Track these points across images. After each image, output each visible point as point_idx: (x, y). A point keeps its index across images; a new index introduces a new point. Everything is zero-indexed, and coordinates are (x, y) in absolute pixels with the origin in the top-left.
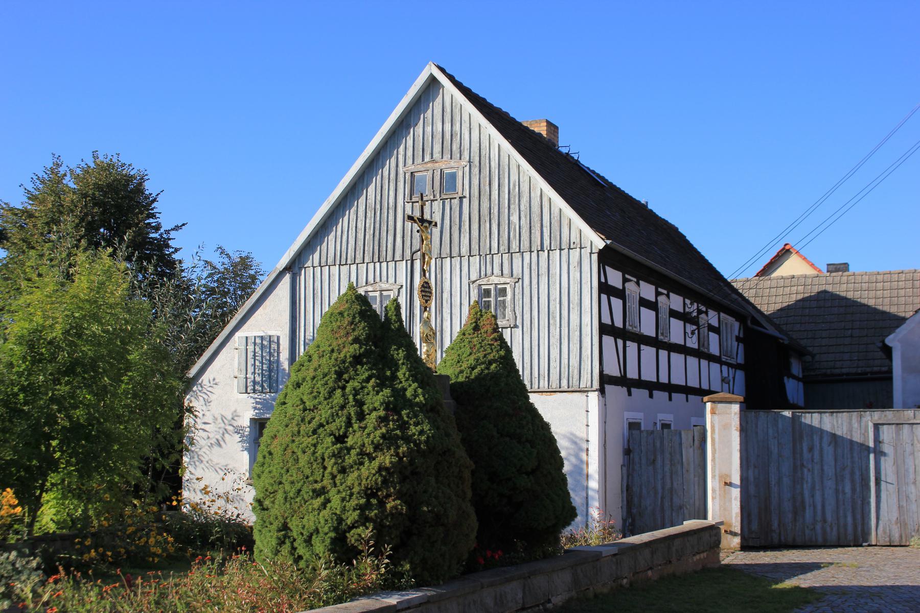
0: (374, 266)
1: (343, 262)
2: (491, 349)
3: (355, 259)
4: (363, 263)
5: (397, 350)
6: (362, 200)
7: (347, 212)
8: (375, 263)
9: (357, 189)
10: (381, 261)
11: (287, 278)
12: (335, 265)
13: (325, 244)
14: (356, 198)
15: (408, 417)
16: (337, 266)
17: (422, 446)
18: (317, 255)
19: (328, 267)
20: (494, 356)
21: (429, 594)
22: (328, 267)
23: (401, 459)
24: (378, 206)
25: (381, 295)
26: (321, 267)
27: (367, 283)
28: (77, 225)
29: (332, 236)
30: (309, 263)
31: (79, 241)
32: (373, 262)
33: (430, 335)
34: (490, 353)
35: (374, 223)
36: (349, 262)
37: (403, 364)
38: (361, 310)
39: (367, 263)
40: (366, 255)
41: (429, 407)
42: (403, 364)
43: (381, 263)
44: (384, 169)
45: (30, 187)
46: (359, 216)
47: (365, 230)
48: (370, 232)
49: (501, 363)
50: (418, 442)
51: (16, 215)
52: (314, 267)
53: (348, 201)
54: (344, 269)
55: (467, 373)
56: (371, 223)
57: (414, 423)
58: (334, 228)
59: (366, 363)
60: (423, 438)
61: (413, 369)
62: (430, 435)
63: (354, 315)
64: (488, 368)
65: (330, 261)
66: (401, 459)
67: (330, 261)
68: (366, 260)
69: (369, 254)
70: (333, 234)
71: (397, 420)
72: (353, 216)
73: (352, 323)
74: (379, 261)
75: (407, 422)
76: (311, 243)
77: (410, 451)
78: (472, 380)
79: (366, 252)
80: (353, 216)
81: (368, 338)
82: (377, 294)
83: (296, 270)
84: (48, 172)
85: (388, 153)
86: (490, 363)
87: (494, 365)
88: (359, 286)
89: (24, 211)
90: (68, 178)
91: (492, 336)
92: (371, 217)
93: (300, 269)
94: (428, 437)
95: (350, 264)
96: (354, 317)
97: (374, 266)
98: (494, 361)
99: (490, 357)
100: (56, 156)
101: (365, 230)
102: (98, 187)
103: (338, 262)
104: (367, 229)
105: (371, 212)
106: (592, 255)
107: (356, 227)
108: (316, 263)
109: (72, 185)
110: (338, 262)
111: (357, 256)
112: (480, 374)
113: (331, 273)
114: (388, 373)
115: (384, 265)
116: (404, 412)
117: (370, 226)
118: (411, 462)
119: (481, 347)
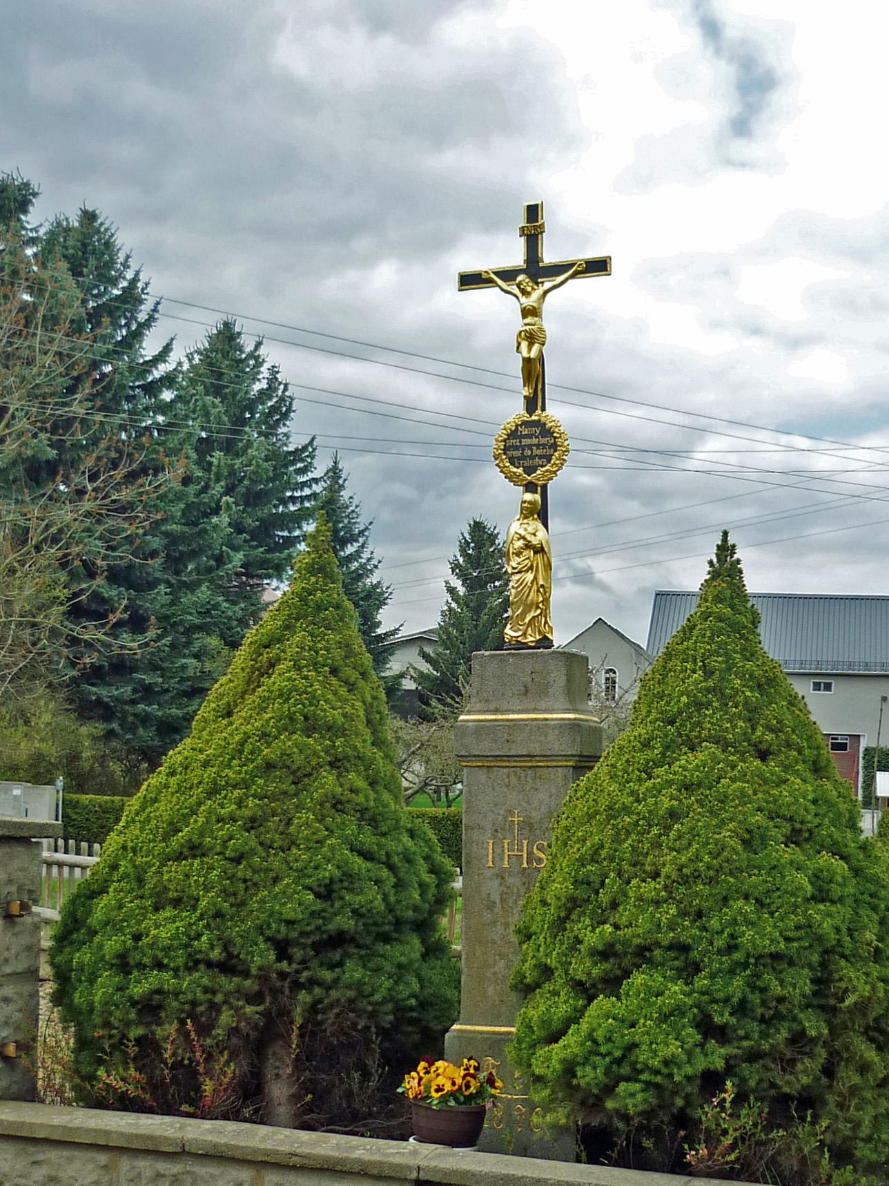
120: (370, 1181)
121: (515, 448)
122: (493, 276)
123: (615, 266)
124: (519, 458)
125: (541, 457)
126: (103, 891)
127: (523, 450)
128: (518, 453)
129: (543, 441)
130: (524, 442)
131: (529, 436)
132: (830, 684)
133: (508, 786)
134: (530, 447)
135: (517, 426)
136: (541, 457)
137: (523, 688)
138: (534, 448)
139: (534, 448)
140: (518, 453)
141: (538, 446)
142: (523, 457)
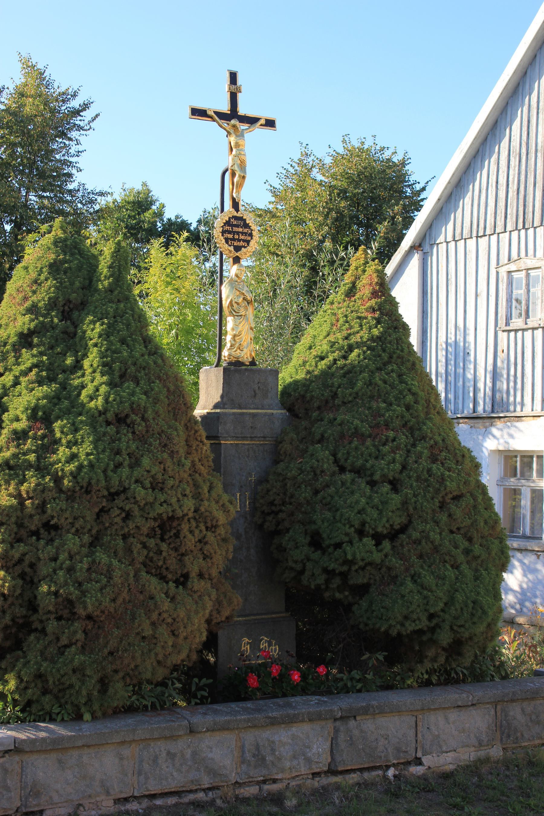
0: (519, 235)
1: (481, 234)
2: (361, 326)
3: (495, 227)
4: (505, 232)
5: (94, 322)
6: (505, 143)
7: (486, 163)
8: (519, 230)
9: (498, 128)
10: (526, 227)
11: (415, 261)
12: (471, 238)
13: (460, 210)
14: (498, 141)
15: (62, 432)
16: (475, 239)
17: (66, 482)
18: (450, 226)
19: (463, 241)
20: (361, 338)
21: (22, 736)
22: (463, 241)
23: (21, 503)
24: (524, 151)
25: (528, 275)
26: (456, 241)
27: (509, 260)
28: (321, 225)
29: (468, 199)
30: (441, 239)
31: (322, 242)
32: (516, 229)
33: (238, 304)
34: (358, 332)
35: (519, 174)
36: (488, 232)
37: (96, 345)
38: (55, 261)
39: (510, 231)
40: (508, 220)
41: (110, 416)
42: (96, 345)
43: (527, 229)
44: (532, 96)
45: (276, 183)
46: (500, 165)
47: (508, 185)
48: (513, 188)
49: (369, 348)
50: (60, 474)
51: (260, 216)
52: (447, 243)
53: (488, 144)
54: (483, 241)
55: (310, 365)
56: (514, 175)
57: (69, 442)
58: (471, 187)
59: (38, 345)
60: (71, 467)
61: (109, 353)
62: (85, 463)
63: (42, 268)
64: (345, 357)
65: (466, 234)
66: (21, 503)
67: (466, 234)
68: (509, 228)
69: (512, 218)
70: (470, 194)
71: (43, 437)
72: (493, 168)
73: (36, 282)
74: (524, 227)
75: (57, 442)
76: (444, 210)
77: (41, 489)
78: (316, 376)
79: (509, 216)
80: (493, 168)
81: (52, 304)
82: (523, 274)
83: (427, 248)
84: (294, 164)
85: (537, 71)
86: (351, 349)
87: (356, 351)
88: (500, 264)
89: (267, 211)
90: (315, 170)
91: (369, 304)
92: (515, 167)
93: (432, 245)
94: (80, 468)
95: (490, 235)
96: (40, 272)
97: (519, 235)
98: (358, 345)
99: (354, 339)
100: (304, 145)
101: (508, 185)
102: (345, 175)
103: (474, 234)
104: (510, 183)
105: (515, 158)
106: (242, 110)
107: (497, 182)
108: (450, 238)
109: (319, 177)
110: (474, 234)
111: (498, 223)
112: (329, 367)
113: (467, 249)
114: (69, 361)
115: (531, 232)
116: (57, 425)
117: (514, 178)
118: (42, 508)
119: (347, 322)
120: (218, 733)
121: (229, 232)
122: (213, 114)
123: (234, 69)
124: (231, 239)
125: (244, 241)
126: (209, 492)
127: (234, 235)
128: (230, 236)
129: (246, 230)
130: (235, 229)
131: (237, 226)
132: (506, 326)
133: (248, 457)
134: (238, 233)
135: (229, 218)
136: (244, 241)
137: (253, 393)
138: (241, 235)
139: (241, 235)
140: (230, 236)
141: (243, 233)
142: (233, 239)
